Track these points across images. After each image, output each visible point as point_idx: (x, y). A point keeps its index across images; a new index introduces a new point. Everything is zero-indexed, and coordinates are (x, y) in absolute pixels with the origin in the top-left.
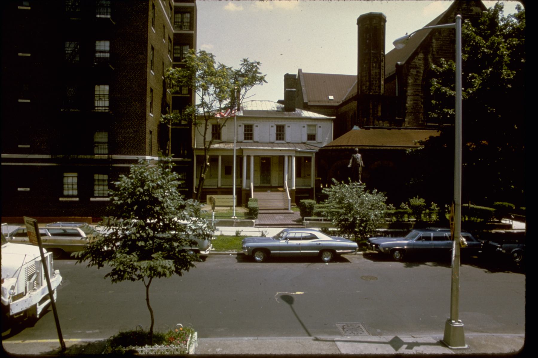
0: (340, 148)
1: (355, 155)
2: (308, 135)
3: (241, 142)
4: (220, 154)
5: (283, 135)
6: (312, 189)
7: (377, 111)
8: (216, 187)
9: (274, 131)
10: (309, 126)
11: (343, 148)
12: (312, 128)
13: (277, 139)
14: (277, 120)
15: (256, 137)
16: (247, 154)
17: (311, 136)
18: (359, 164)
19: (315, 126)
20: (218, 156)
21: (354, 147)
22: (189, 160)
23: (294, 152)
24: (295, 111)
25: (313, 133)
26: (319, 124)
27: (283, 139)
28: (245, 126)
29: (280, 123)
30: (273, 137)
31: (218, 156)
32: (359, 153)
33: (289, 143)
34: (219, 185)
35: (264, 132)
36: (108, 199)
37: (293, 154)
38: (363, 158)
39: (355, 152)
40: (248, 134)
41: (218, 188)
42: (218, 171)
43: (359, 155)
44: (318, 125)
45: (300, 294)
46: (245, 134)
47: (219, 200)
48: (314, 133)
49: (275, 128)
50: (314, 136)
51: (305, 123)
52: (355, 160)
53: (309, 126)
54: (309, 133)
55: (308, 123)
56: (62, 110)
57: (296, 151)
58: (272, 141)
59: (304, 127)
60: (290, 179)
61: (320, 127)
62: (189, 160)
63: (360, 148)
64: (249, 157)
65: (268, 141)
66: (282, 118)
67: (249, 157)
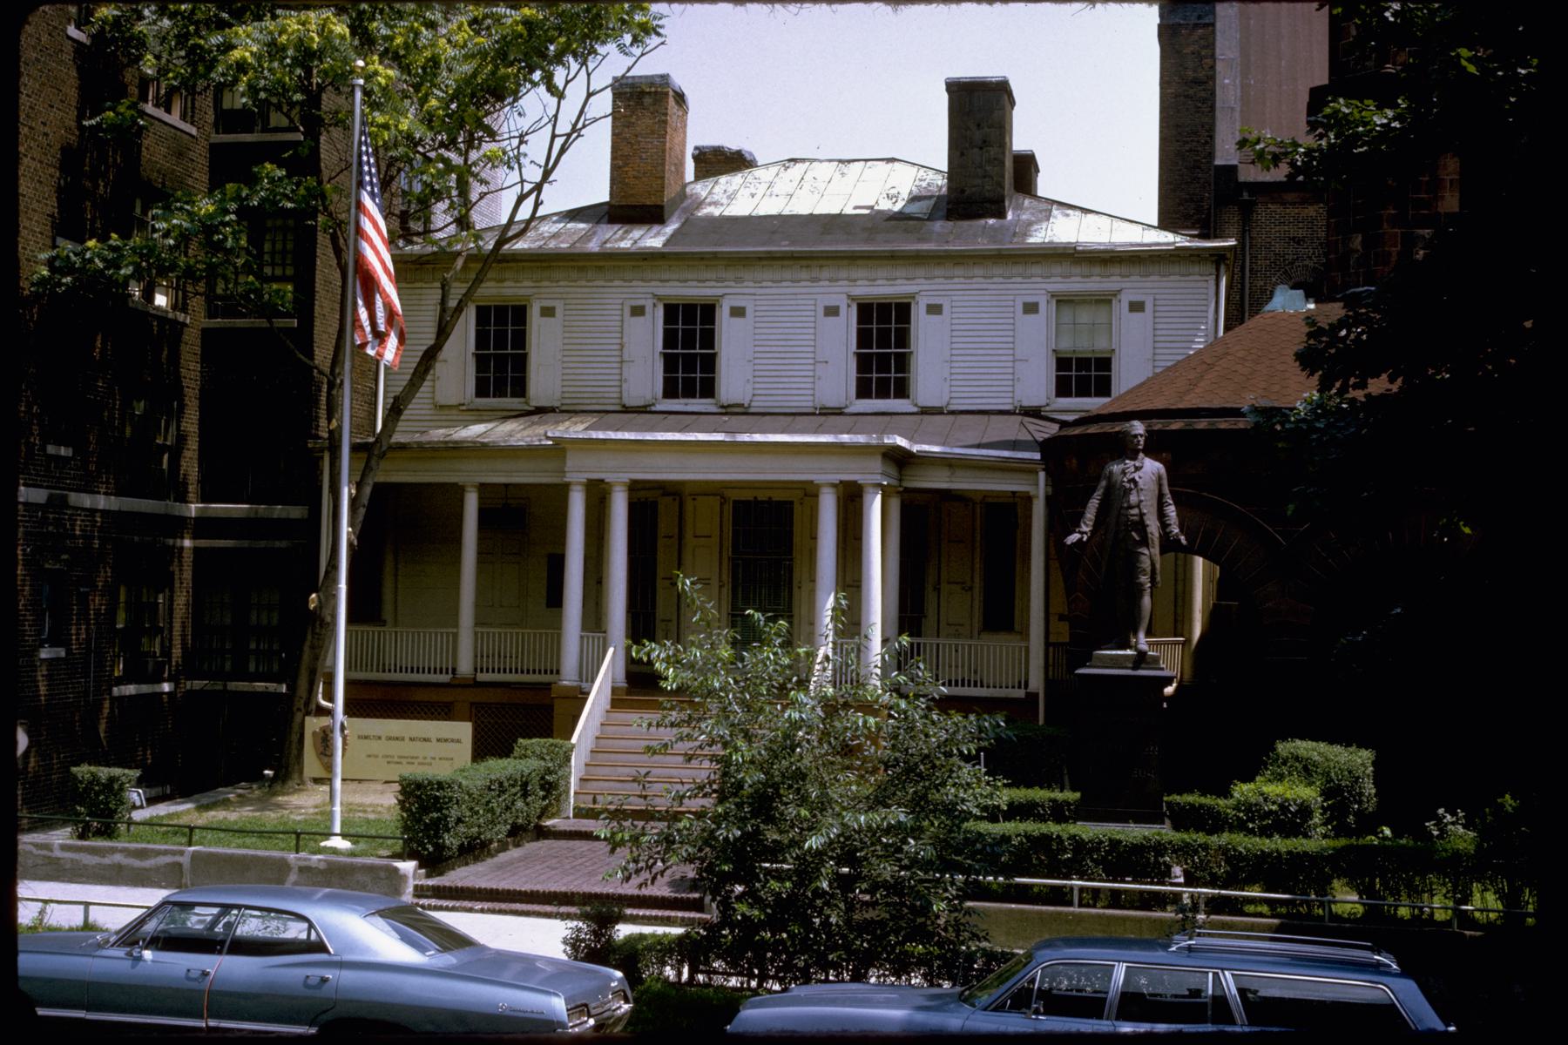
0: (1176, 425)
1: (1116, 468)
2: (1062, 363)
4: (470, 475)
5: (903, 363)
6: (1032, 697)
8: (444, 678)
9: (842, 336)
10: (1063, 301)
11: (1202, 424)
12: (1085, 316)
13: (863, 391)
14: (859, 273)
15: (733, 382)
17: (1083, 363)
18: (1141, 526)
19: (1104, 300)
20: (457, 491)
22: (296, 512)
23: (877, 464)
24: (1001, 214)
25: (1084, 344)
26: (1131, 287)
27: (902, 391)
28: (671, 311)
29: (884, 286)
30: (644, 375)
31: (457, 491)
32: (1151, 451)
34: (465, 667)
35: (788, 348)
37: (871, 473)
38: (1179, 480)
39: (1123, 448)
40: (689, 362)
41: (458, 684)
43: (1151, 468)
44: (1126, 298)
45: (300, 1037)
46: (670, 363)
48: (1100, 345)
49: (655, 323)
50: (1105, 363)
51: (1041, 286)
52: (1116, 496)
53: (1063, 301)
54: (1067, 345)
57: (900, 460)
58: (634, 397)
59: (1031, 308)
60: (851, 622)
61: (1137, 307)
62: (296, 512)
63: (1158, 425)
64: (598, 496)
65: (805, 403)
67: (598, 496)
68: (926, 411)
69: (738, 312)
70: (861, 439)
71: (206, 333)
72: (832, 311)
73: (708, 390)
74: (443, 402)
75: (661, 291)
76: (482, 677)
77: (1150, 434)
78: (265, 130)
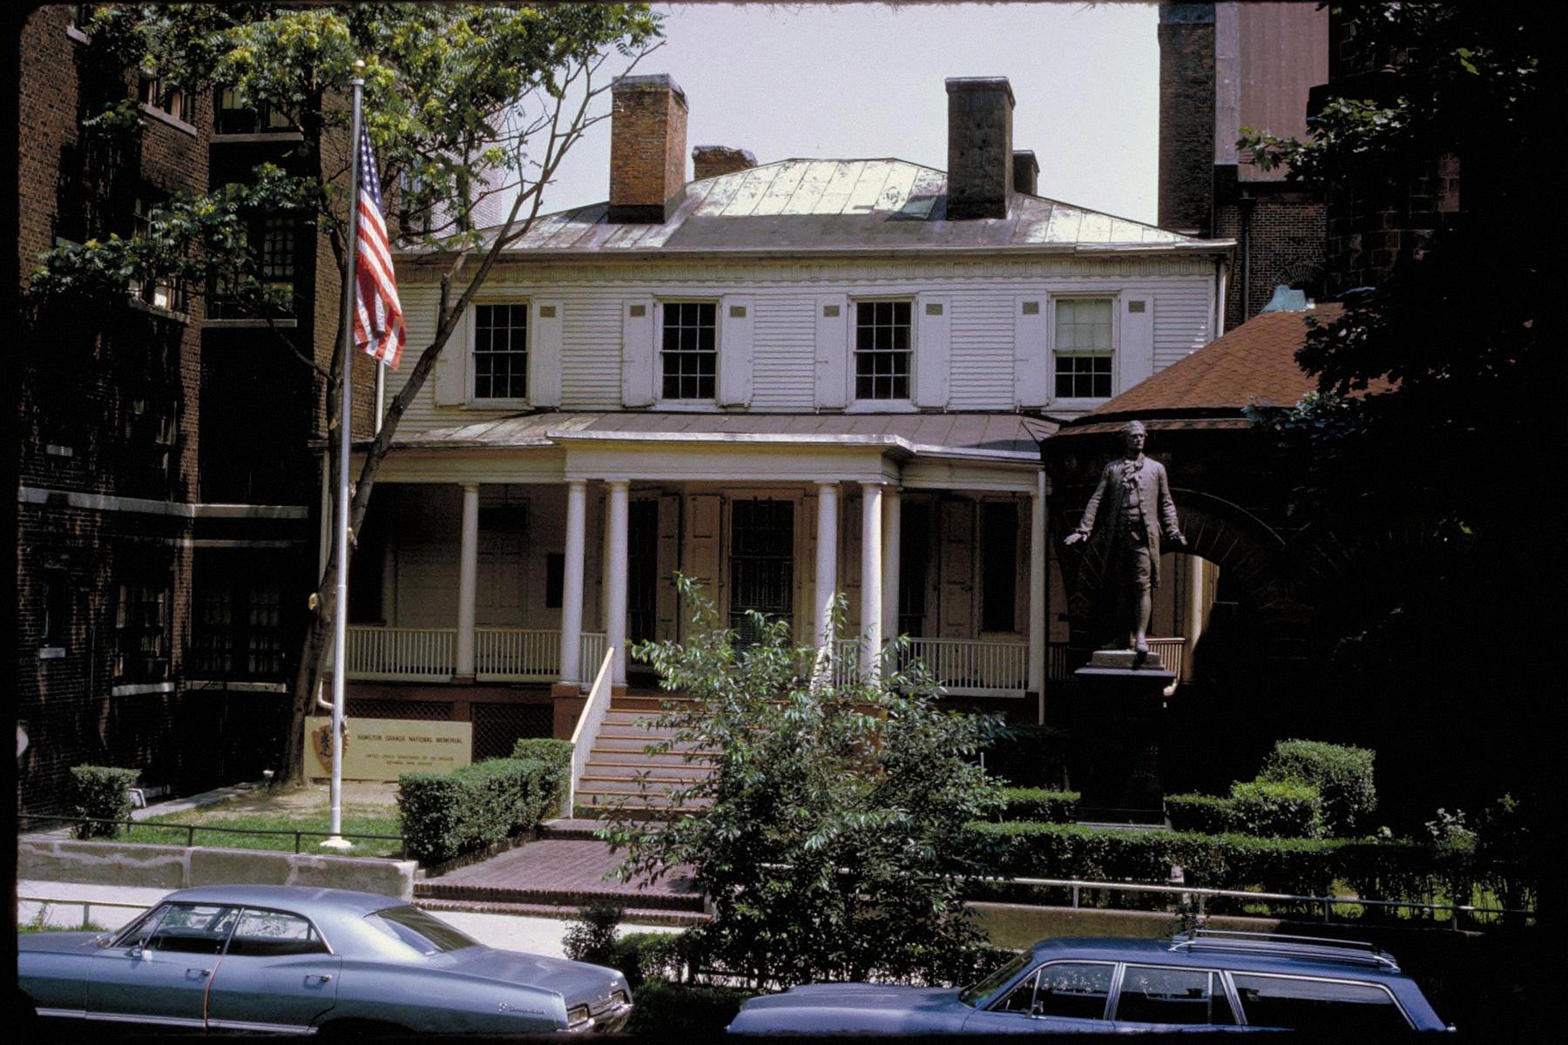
1: (1116, 468)
2: (1063, 363)
3: (643, 410)
4: (470, 475)
5: (903, 363)
7: (1436, 185)
8: (445, 678)
9: (842, 335)
10: (1063, 301)
12: (1085, 315)
13: (863, 391)
14: (860, 272)
16: (583, 477)
17: (1083, 363)
18: (1141, 526)
19: (1104, 300)
20: (457, 492)
21: (1118, 427)
22: (296, 512)
23: (877, 464)
24: (1001, 214)
25: (1084, 345)
26: (1131, 286)
27: (902, 390)
28: (671, 311)
29: (884, 286)
30: (836, 375)
31: (457, 492)
33: (937, 411)
34: (465, 667)
35: (789, 349)
36: (969, 904)
37: (872, 473)
39: (1122, 448)
40: (689, 362)
42: (456, 586)
43: (1150, 469)
44: (1126, 298)
46: (670, 363)
47: (375, 746)
48: (1099, 346)
49: (846, 328)
50: (1105, 363)
51: (1041, 286)
52: (1115, 497)
53: (1063, 301)
54: (1067, 345)
55: (1060, 286)
56: (1528, 324)
59: (1031, 308)
61: (1137, 307)
62: (296, 512)
63: (1158, 425)
64: (598, 496)
65: (805, 403)
66: (893, 258)
67: (598, 496)
68: (925, 411)
72: (832, 311)
73: (708, 390)
75: (660, 292)
76: (482, 677)
77: (1150, 433)
78: (265, 130)
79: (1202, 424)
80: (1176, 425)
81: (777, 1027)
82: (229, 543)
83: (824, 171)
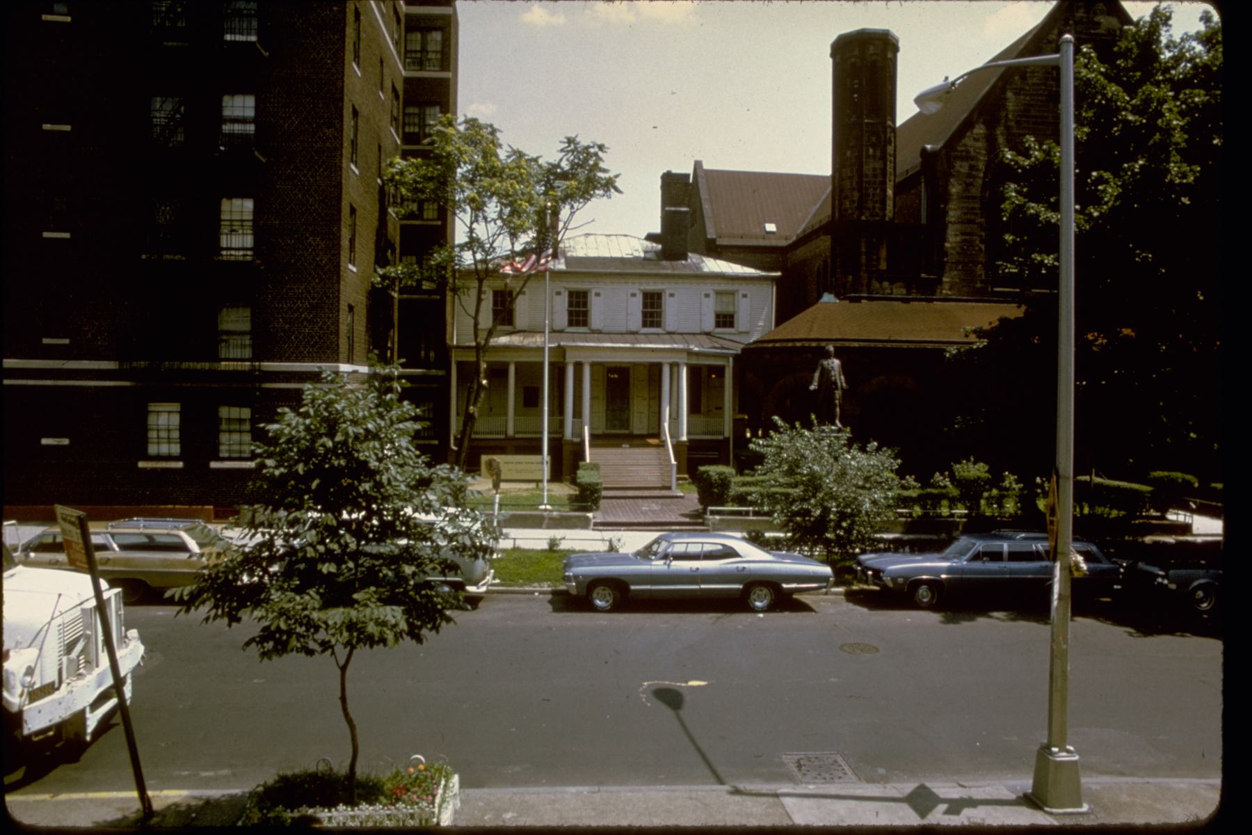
1: (825, 363)
2: (718, 316)
3: (561, 331)
4: (512, 359)
5: (659, 315)
7: (878, 260)
8: (502, 437)
9: (637, 305)
10: (718, 293)
12: (725, 298)
13: (645, 325)
14: (643, 281)
15: (596, 320)
17: (725, 316)
18: (835, 383)
19: (733, 293)
20: (506, 365)
21: (823, 344)
22: (441, 373)
23: (685, 355)
24: (686, 259)
25: (727, 309)
26: (742, 288)
27: (658, 325)
28: (571, 294)
29: (652, 286)
30: (635, 320)
31: (506, 365)
32: (836, 356)
33: (673, 333)
34: (511, 432)
35: (615, 308)
36: (251, 465)
37: (682, 359)
38: (845, 368)
39: (827, 355)
40: (578, 313)
41: (508, 439)
42: (506, 399)
43: (836, 362)
44: (741, 292)
46: (570, 313)
47: (510, 466)
48: (730, 309)
49: (639, 299)
50: (732, 316)
51: (710, 288)
52: (826, 373)
53: (718, 293)
54: (719, 309)
57: (690, 353)
58: (634, 329)
59: (707, 296)
60: (675, 419)
61: (745, 296)
62: (441, 373)
63: (838, 344)
64: (578, 366)
65: (623, 330)
66: (657, 275)
67: (578, 366)
69: (598, 295)
70: (667, 346)
71: (400, 301)
72: (634, 295)
73: (585, 323)
74: (556, 328)
79: (798, 344)
80: (790, 344)
81: (760, 570)
82: (185, 365)
83: (600, 239)
